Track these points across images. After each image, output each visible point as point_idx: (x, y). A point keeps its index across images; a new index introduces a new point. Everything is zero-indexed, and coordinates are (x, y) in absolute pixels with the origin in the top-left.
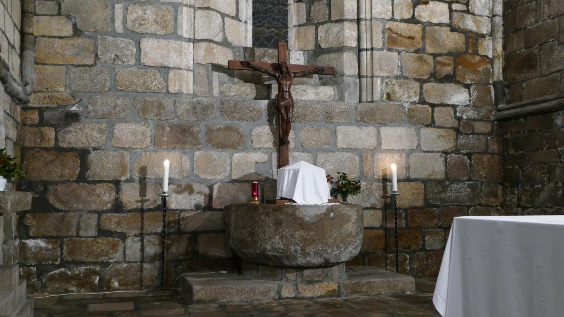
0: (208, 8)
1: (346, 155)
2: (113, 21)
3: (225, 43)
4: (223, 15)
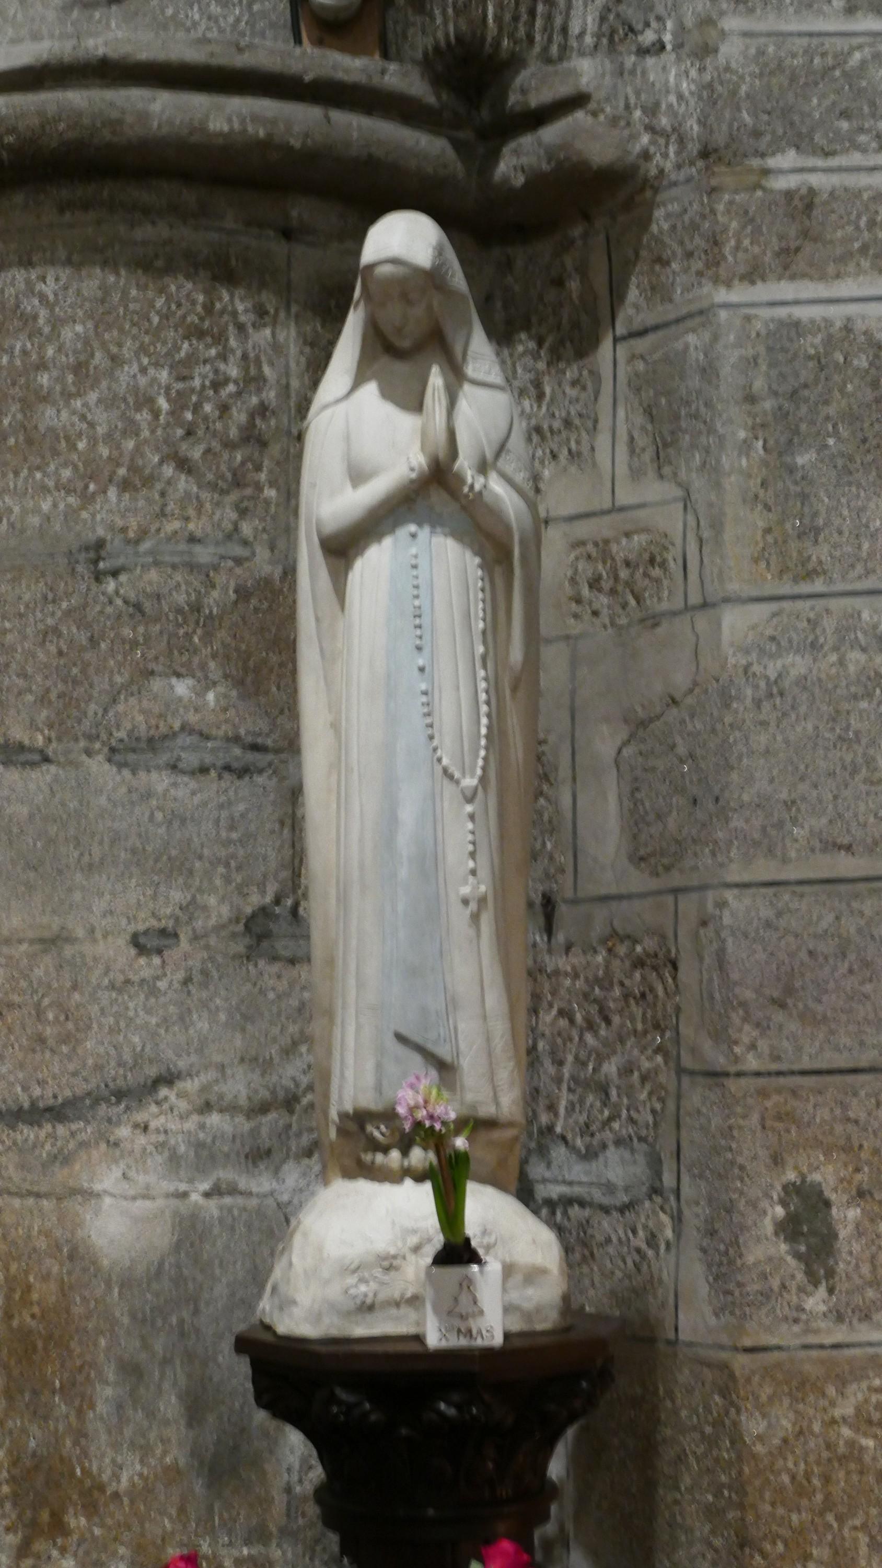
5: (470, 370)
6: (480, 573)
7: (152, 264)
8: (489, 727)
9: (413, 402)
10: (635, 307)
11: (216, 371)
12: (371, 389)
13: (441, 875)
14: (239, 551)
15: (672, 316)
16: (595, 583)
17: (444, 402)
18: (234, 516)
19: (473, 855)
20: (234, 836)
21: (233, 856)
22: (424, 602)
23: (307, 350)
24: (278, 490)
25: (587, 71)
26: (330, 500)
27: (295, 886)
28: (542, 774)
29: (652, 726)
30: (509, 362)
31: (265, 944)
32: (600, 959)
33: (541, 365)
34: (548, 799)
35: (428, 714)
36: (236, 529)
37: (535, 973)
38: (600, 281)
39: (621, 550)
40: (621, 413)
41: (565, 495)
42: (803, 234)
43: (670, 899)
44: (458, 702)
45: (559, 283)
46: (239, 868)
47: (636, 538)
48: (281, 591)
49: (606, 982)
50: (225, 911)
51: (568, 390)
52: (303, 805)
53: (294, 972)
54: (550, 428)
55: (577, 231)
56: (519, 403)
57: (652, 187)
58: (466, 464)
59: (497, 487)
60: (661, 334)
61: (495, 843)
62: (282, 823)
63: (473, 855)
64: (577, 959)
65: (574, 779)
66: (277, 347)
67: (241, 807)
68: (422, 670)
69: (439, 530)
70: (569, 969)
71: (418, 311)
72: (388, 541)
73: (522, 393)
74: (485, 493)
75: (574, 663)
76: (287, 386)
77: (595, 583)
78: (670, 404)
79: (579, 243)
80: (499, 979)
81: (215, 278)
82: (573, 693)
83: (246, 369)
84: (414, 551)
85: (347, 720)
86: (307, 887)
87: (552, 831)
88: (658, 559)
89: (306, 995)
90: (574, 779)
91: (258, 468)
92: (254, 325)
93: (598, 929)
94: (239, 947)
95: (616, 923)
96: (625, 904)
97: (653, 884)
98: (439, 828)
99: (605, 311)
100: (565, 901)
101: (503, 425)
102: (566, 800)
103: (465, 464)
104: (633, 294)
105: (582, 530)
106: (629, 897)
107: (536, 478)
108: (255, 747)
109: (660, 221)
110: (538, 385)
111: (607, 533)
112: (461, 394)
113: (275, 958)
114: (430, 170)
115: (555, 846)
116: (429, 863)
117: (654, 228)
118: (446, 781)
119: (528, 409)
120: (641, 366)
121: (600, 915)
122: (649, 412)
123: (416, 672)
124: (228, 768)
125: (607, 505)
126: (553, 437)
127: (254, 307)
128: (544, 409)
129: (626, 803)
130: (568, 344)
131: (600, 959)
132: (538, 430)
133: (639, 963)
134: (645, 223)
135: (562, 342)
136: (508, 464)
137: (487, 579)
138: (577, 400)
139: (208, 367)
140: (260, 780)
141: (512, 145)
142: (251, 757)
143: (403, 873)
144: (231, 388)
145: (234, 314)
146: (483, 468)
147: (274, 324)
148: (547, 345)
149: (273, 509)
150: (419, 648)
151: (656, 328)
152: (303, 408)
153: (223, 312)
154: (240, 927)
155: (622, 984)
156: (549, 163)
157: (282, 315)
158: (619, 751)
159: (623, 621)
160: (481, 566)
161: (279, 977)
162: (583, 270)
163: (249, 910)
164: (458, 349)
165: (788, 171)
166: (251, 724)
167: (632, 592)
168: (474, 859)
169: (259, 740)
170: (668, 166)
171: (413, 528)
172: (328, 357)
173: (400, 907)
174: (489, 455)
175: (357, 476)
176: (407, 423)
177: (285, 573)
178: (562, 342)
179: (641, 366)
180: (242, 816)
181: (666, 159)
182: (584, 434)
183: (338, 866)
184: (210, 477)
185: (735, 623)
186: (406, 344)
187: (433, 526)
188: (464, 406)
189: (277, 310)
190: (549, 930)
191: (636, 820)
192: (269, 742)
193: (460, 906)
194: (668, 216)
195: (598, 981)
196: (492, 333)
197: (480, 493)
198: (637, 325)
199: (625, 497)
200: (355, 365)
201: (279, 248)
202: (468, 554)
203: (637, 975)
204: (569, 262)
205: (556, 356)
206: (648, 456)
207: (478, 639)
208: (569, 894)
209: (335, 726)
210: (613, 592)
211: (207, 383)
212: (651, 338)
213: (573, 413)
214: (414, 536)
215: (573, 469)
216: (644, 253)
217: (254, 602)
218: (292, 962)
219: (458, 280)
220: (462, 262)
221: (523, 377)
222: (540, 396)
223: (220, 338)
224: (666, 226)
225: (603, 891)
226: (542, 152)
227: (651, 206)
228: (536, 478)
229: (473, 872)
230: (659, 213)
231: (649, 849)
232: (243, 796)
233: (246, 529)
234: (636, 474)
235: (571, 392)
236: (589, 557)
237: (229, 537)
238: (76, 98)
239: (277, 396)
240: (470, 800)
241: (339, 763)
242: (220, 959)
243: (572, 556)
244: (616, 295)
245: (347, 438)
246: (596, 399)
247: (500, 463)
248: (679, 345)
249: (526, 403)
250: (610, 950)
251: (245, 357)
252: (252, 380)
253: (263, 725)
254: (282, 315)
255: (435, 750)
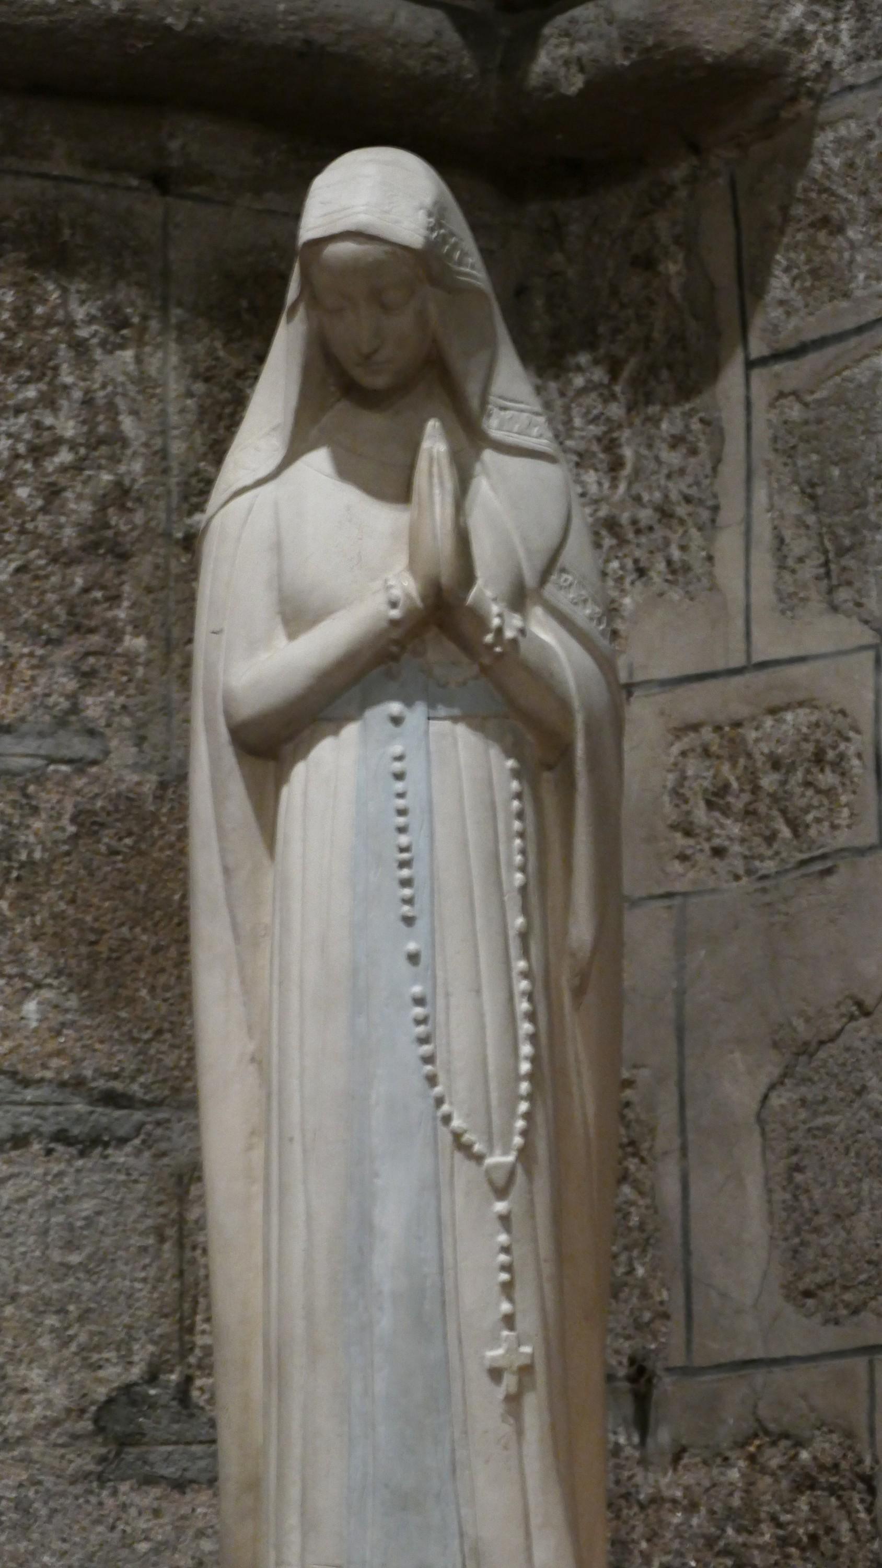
5: (494, 427)
6: (515, 785)
8: (534, 1060)
9: (393, 483)
10: (784, 305)
11: (38, 426)
12: (318, 461)
13: (452, 1328)
14: (80, 747)
15: (850, 323)
16: (716, 798)
17: (449, 485)
18: (71, 685)
19: (508, 1289)
20: (74, 1258)
21: (72, 1296)
22: (415, 838)
23: (199, 387)
24: (149, 636)
26: (250, 655)
27: (186, 1350)
28: (629, 1146)
29: (822, 1054)
30: (559, 403)
31: (131, 1453)
32: (734, 1474)
33: (616, 410)
34: (636, 1185)
35: (424, 1040)
36: (75, 709)
37: (620, 1500)
38: (720, 261)
39: (763, 738)
40: (761, 495)
41: (662, 642)
43: (860, 1364)
44: (481, 1019)
45: (647, 263)
46: (82, 1318)
47: (789, 716)
48: (155, 815)
49: (747, 1517)
50: (58, 1392)
51: (666, 455)
52: (201, 1199)
53: (183, 1504)
54: (634, 522)
55: (678, 173)
56: (578, 481)
57: (810, 93)
58: (489, 593)
59: (544, 632)
60: (830, 352)
61: (548, 1269)
62: (162, 1239)
63: (508, 1289)
64: (693, 1476)
65: (684, 1150)
66: (143, 382)
67: (87, 1206)
68: (413, 958)
69: (442, 711)
70: (679, 1494)
71: (402, 323)
72: (351, 731)
73: (582, 460)
74: (523, 643)
75: (682, 943)
76: (163, 453)
77: (716, 798)
78: (846, 476)
79: (682, 193)
80: (557, 1515)
81: (33, 262)
82: (680, 993)
83: (90, 423)
84: (397, 749)
85: (282, 1051)
86: (208, 1351)
87: (645, 1245)
88: (831, 755)
89: (207, 1545)
90: (684, 1150)
91: (114, 599)
92: (103, 344)
93: (732, 1421)
94: (83, 1461)
95: (763, 1412)
96: (778, 1373)
97: (830, 1339)
98: (448, 1239)
99: (728, 308)
100: (669, 1370)
101: (554, 522)
102: (670, 1189)
103: (487, 593)
104: (779, 284)
105: (696, 702)
106: (786, 1361)
107: (612, 611)
108: (111, 1099)
109: (827, 154)
110: (611, 445)
111: (741, 710)
112: (478, 467)
113: (149, 1480)
114: (414, 65)
115: (653, 1270)
116: (431, 1306)
117: (816, 167)
118: (458, 1156)
119: (593, 489)
120: (795, 412)
121: (736, 1394)
122: (810, 493)
123: (404, 965)
124: (62, 1137)
125: (738, 660)
126: (641, 537)
127: (102, 310)
128: (622, 487)
129: (781, 1196)
130: (665, 374)
131: (734, 1474)
132: (612, 525)
133: (806, 1483)
134: (799, 157)
135: (652, 369)
136: (561, 593)
137: (527, 797)
138: (682, 472)
139: (22, 419)
140: (119, 1156)
141: (561, 21)
142: (105, 1115)
143: (385, 1323)
144: (65, 456)
145: (69, 325)
146: (519, 599)
147: (140, 343)
148: (626, 374)
149: (140, 672)
150: (409, 921)
151: (821, 343)
152: (198, 491)
153: (49, 322)
154: (86, 1425)
155: (774, 1519)
156: (627, 50)
157: (154, 325)
158: (766, 1097)
159: (769, 866)
160: (516, 774)
161: (157, 1513)
162: (688, 241)
163: (101, 1393)
164: (472, 389)
166: (103, 1057)
167: (784, 812)
168: (511, 1299)
169: (118, 1085)
170: (840, 56)
171: (395, 707)
172: (240, 402)
173: (380, 1386)
174: (530, 579)
175: (296, 616)
176: (383, 520)
177: (163, 785)
178: (652, 369)
179: (795, 412)
180: (89, 1222)
182: (693, 531)
183: (267, 1313)
184: (27, 614)
186: (380, 381)
187: (432, 705)
188: (482, 486)
189: (145, 317)
190: (642, 1423)
191: (797, 1224)
192: (135, 1088)
193: (486, 1380)
194: (841, 144)
195: (731, 1514)
196: (526, 356)
197: (514, 641)
198: (786, 340)
199: (767, 647)
200: (290, 419)
201: (149, 209)
202: (495, 752)
203: (803, 1504)
204: (662, 225)
205: (642, 395)
206: (809, 571)
207: (513, 903)
208: (677, 1359)
209: (259, 1061)
210: (749, 813)
211: (21, 448)
212: (813, 360)
213: (674, 496)
214: (397, 721)
215: (675, 595)
216: (798, 210)
217: (107, 838)
218: (180, 1485)
219: (472, 268)
220: (475, 227)
221: (586, 432)
222: (616, 465)
223: (44, 369)
224: (836, 163)
225: (740, 1353)
226: (614, 33)
227: (812, 126)
228: (612, 611)
229: (509, 1321)
230: (824, 139)
231: (819, 1277)
232: (88, 1183)
233: (94, 707)
234: (788, 602)
235: (673, 458)
236: (706, 752)
237: (62, 722)
239: (147, 471)
240: (501, 1193)
241: (267, 1126)
242: (49, 1481)
243: (675, 749)
244: (750, 285)
245: (278, 548)
246: (714, 469)
247: (550, 590)
248: (861, 373)
249: (591, 477)
250: (752, 1459)
251: (88, 401)
252: (103, 442)
253: (125, 1058)
254: (154, 325)
255: (439, 1101)
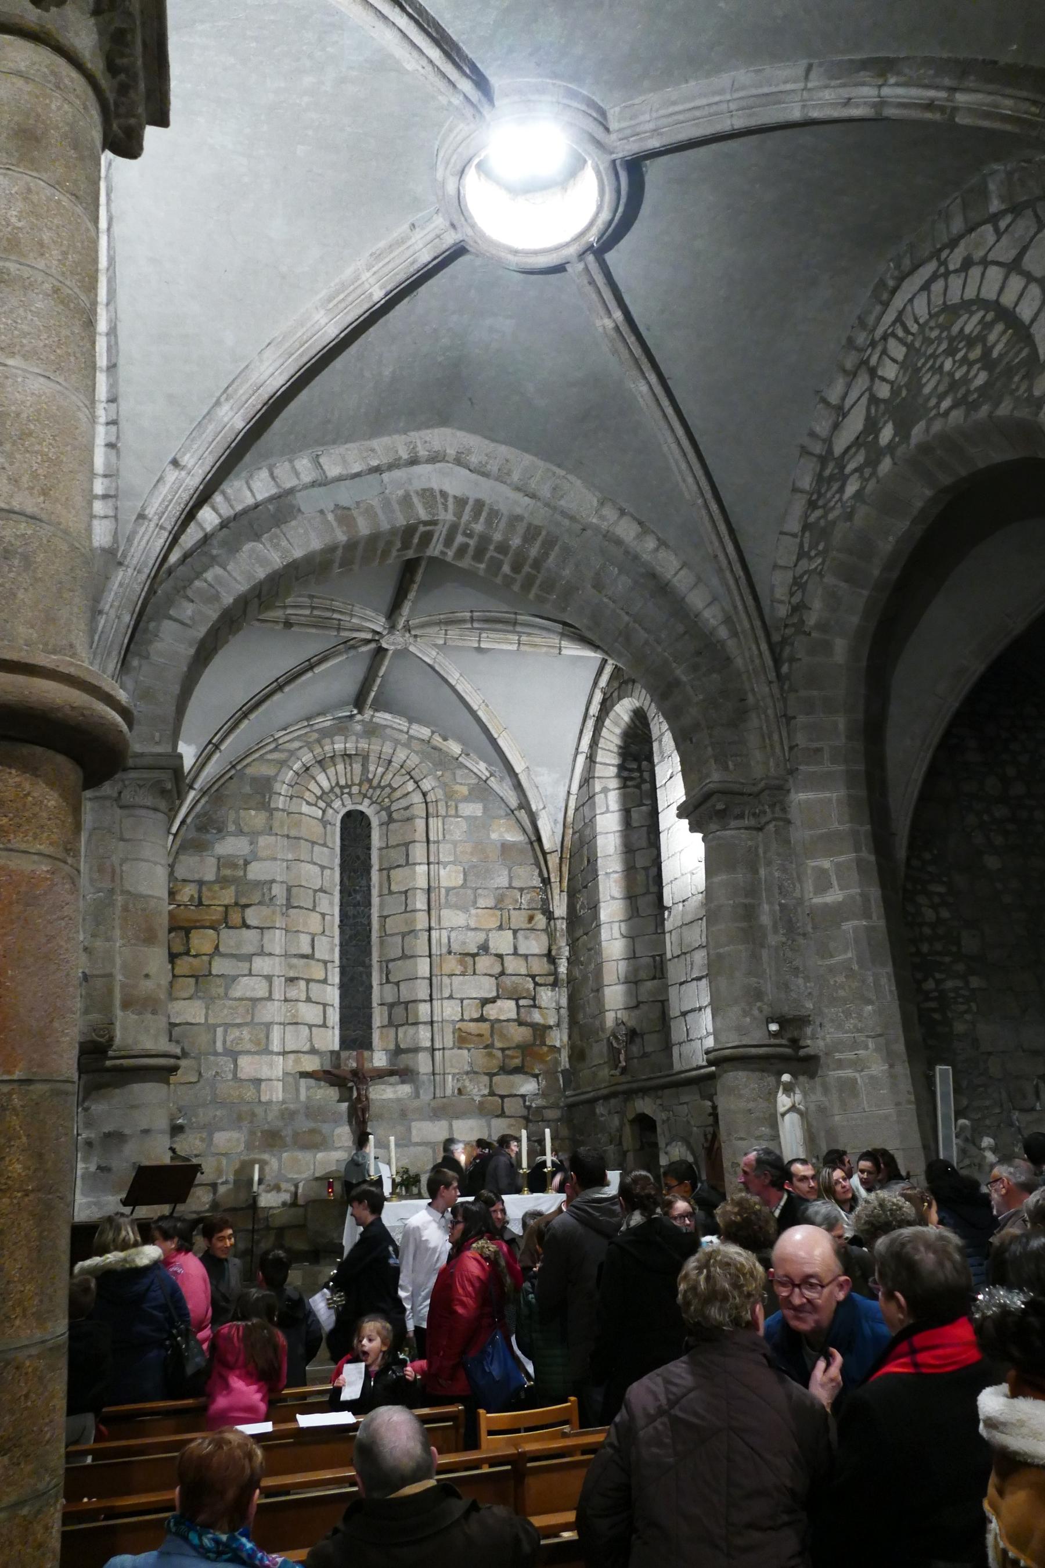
0: (296, 1023)
1: (420, 1148)
2: (215, 1042)
3: (313, 1051)
4: (310, 1026)
7: (753, 1070)
9: (789, 1097)
10: (820, 1073)
25: (809, 1042)
42: (840, 1064)
165: (838, 1056)
181: (821, 1054)
185: (837, 1118)
238: (741, 1050)
